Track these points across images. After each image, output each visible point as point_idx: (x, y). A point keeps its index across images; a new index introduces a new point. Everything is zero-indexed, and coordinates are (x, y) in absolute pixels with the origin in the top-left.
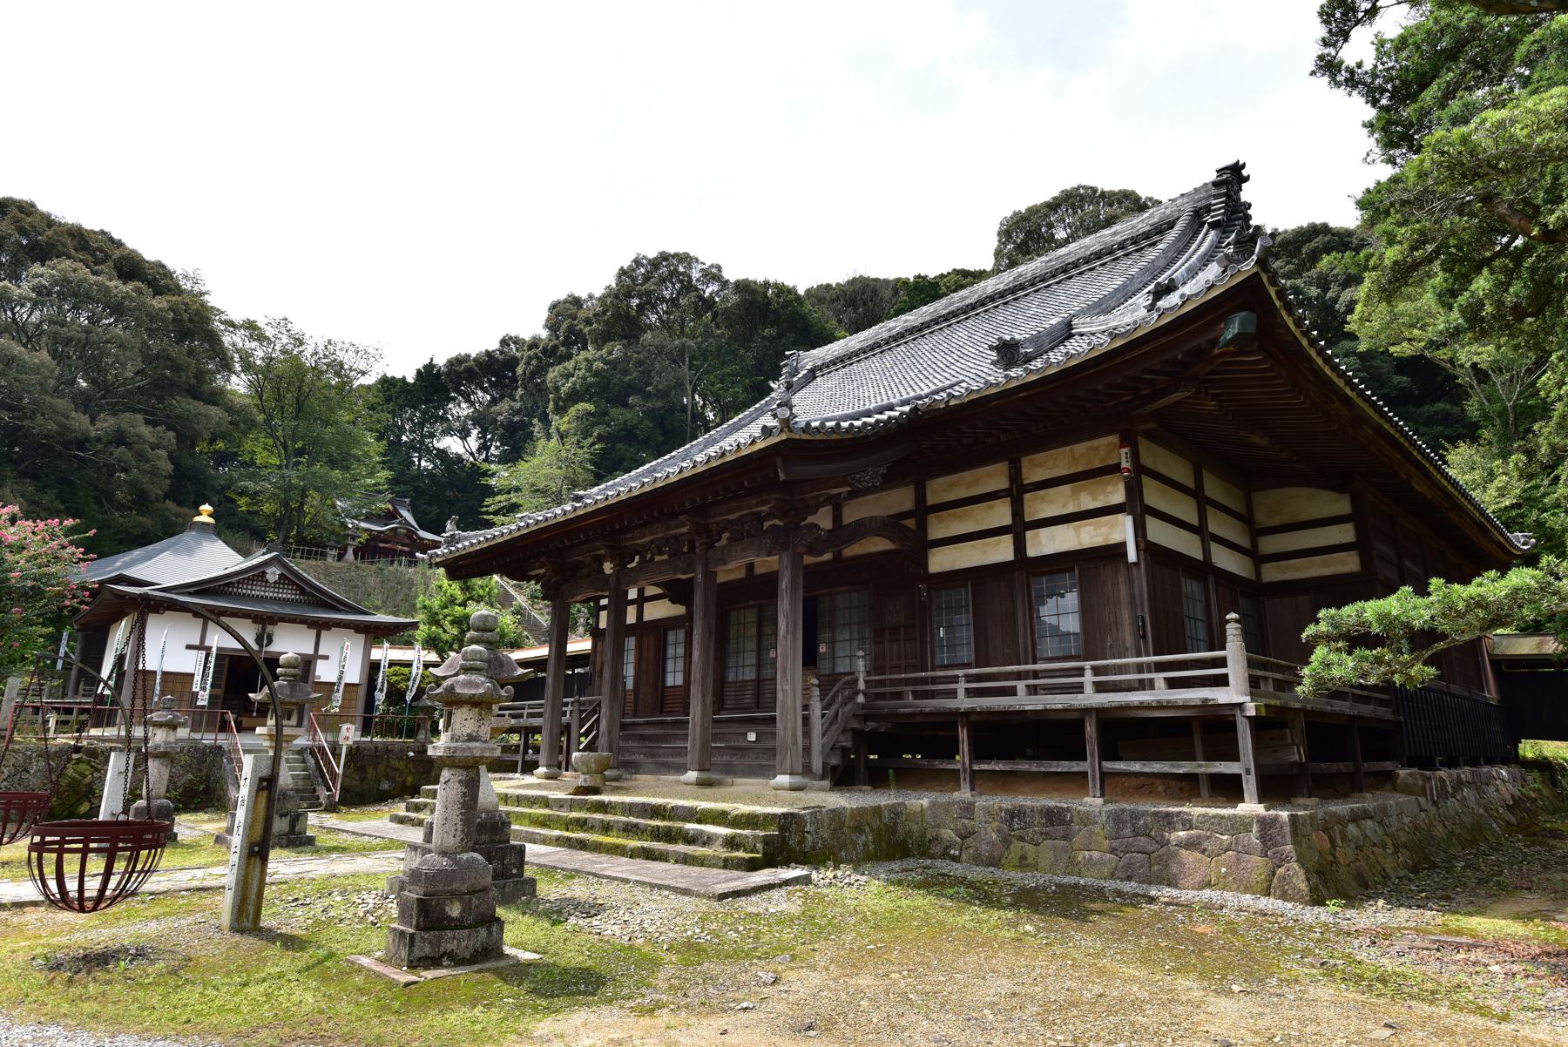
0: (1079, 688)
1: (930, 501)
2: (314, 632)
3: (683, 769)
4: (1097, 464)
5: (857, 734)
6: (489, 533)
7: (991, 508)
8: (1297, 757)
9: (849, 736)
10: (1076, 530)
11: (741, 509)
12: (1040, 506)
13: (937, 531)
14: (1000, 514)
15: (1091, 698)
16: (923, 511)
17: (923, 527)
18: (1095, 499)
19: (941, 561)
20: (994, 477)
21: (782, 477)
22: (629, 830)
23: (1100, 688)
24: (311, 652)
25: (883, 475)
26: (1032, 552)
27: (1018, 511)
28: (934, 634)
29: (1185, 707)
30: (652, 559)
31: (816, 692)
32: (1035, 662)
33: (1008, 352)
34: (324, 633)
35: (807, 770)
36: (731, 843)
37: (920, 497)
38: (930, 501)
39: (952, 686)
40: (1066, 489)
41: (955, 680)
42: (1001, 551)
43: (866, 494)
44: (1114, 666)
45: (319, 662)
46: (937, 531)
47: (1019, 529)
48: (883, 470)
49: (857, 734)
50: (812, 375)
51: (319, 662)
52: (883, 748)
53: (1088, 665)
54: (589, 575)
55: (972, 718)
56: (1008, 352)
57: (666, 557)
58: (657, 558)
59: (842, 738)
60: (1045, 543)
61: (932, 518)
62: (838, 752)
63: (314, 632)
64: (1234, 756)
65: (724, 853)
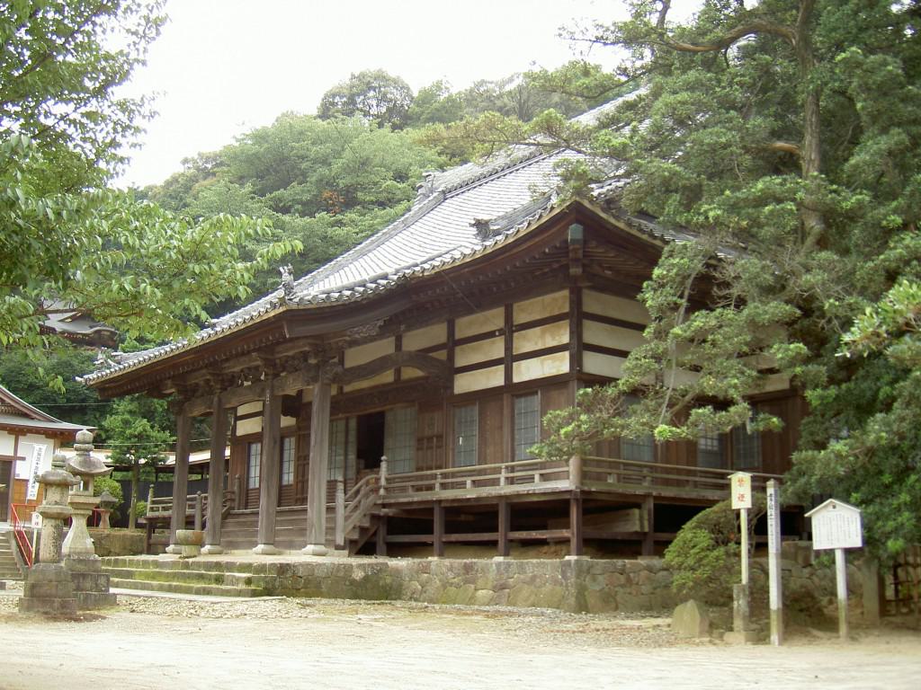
0: (495, 482)
1: (458, 335)
2: (13, 437)
3: (255, 544)
4: (556, 312)
5: (374, 517)
6: (204, 333)
7: (493, 343)
8: (637, 528)
9: (368, 519)
10: (542, 363)
11: (292, 348)
12: (525, 343)
13: (460, 361)
14: (497, 349)
15: (504, 489)
16: (453, 343)
17: (451, 358)
18: (553, 339)
19: (465, 384)
20: (493, 318)
21: (288, 336)
22: (201, 577)
23: (511, 481)
24: (11, 453)
25: (380, 327)
26: (516, 379)
27: (509, 348)
28: (455, 441)
29: (544, 494)
30: (242, 384)
31: (341, 486)
32: (513, 461)
33: (482, 227)
34: (20, 437)
35: (328, 543)
36: (249, 581)
37: (509, 317)
38: (458, 335)
39: (433, 482)
40: (538, 330)
41: (434, 477)
42: (496, 378)
43: (365, 343)
44: (490, 469)
45: (18, 462)
46: (460, 361)
47: (509, 360)
48: (381, 323)
49: (374, 517)
50: (445, 195)
51: (18, 462)
52: (399, 531)
53: (503, 465)
54: (202, 395)
55: (443, 505)
56: (482, 227)
57: (250, 383)
58: (246, 384)
59: (364, 520)
60: (527, 371)
61: (458, 349)
62: (357, 530)
63: (13, 437)
64: (567, 526)
65: (242, 586)
